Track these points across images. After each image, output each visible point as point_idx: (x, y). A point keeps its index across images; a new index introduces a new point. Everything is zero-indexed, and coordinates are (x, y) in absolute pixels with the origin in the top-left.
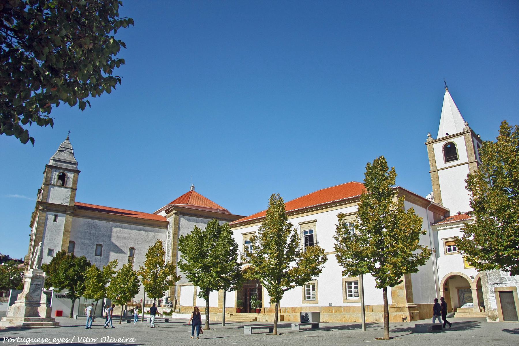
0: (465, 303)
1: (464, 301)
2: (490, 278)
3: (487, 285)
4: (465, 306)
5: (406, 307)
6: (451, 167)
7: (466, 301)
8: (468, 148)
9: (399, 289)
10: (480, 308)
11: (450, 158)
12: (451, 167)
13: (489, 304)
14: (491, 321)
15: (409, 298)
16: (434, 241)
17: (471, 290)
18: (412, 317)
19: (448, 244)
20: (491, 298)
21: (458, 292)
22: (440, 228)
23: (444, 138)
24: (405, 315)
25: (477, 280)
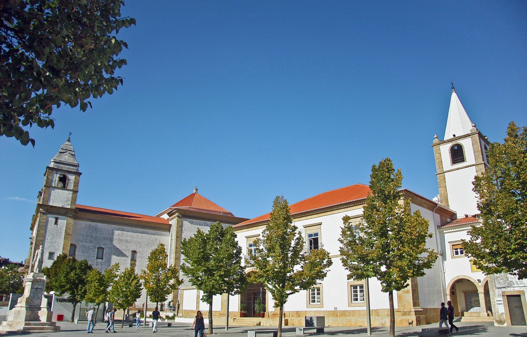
0: (472, 307)
1: (471, 305)
3: (494, 289)
6: (458, 169)
7: (474, 305)
8: (476, 150)
9: (405, 293)
10: (487, 312)
12: (458, 169)
13: (496, 307)
17: (478, 294)
18: (418, 321)
20: (498, 302)
21: (465, 296)
22: (447, 231)
23: (451, 139)
25: (484, 284)
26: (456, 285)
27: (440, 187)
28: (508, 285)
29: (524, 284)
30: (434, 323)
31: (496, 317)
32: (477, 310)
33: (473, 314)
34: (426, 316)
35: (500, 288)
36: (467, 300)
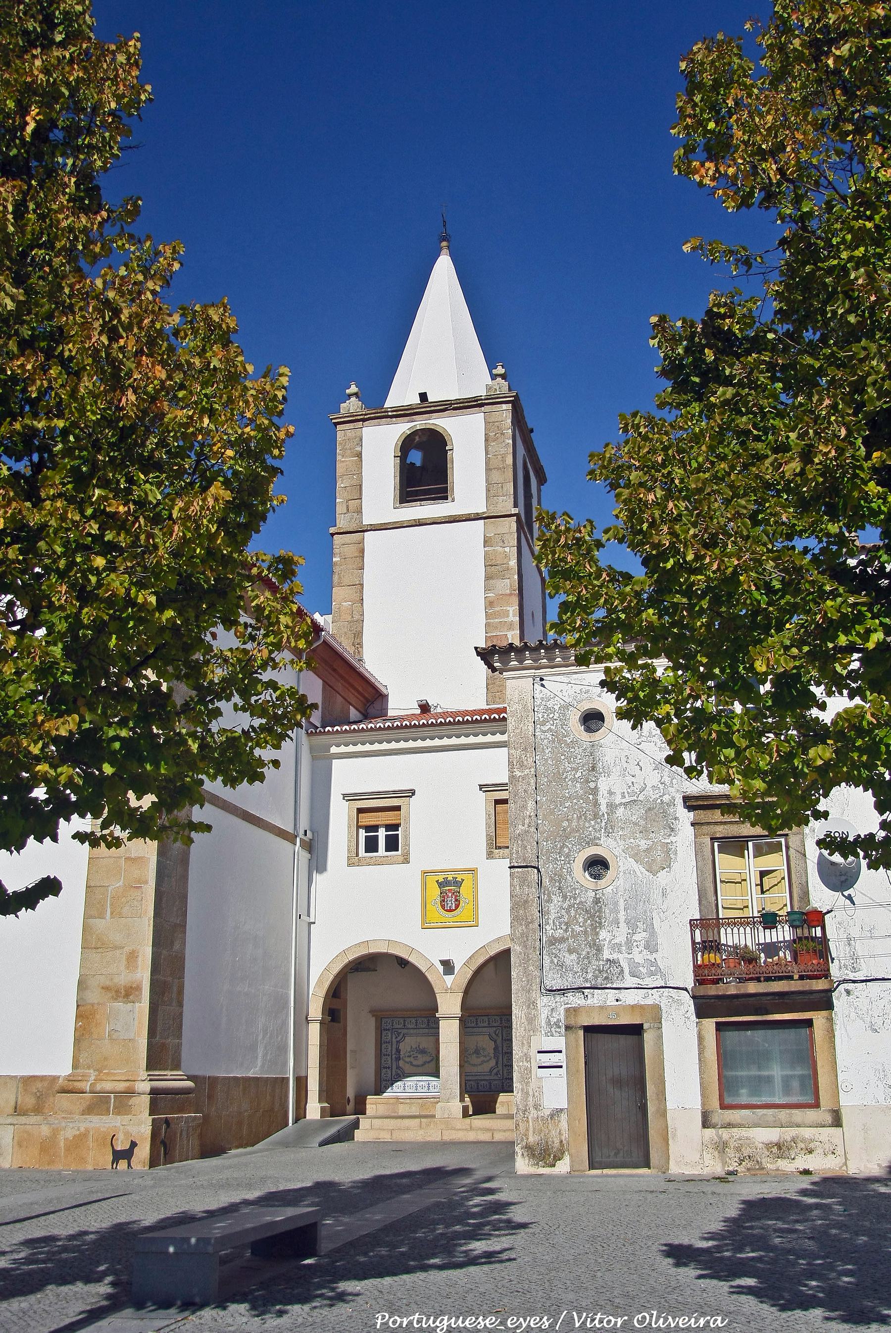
0: (400, 1076)
1: (398, 1067)
2: (552, 962)
4: (397, 1089)
5: (140, 1090)
6: (419, 523)
7: (407, 1068)
8: (495, 463)
9: (115, 999)
10: (462, 1100)
11: (417, 493)
12: (419, 523)
13: (533, 1085)
14: (533, 1170)
15: (164, 1045)
16: (312, 808)
17: (437, 1021)
18: (163, 1143)
19: (369, 819)
20: (546, 1059)
21: (380, 1030)
22: (343, 749)
23: (410, 407)
24: (127, 1134)
25: (466, 981)
26: (349, 985)
27: (340, 585)
28: (596, 977)
29: (663, 976)
30: (237, 1147)
31: (527, 1130)
32: (420, 1089)
33: (401, 1106)
34: (206, 1118)
35: (563, 991)
36: (384, 1046)
